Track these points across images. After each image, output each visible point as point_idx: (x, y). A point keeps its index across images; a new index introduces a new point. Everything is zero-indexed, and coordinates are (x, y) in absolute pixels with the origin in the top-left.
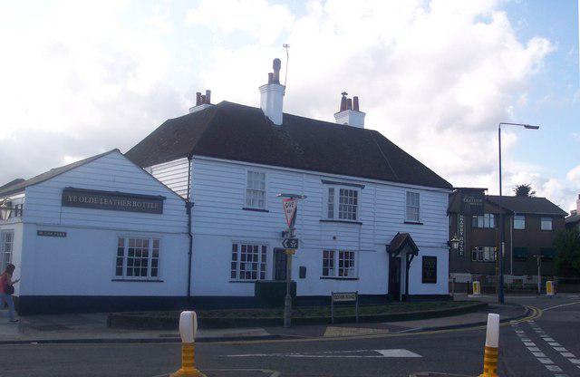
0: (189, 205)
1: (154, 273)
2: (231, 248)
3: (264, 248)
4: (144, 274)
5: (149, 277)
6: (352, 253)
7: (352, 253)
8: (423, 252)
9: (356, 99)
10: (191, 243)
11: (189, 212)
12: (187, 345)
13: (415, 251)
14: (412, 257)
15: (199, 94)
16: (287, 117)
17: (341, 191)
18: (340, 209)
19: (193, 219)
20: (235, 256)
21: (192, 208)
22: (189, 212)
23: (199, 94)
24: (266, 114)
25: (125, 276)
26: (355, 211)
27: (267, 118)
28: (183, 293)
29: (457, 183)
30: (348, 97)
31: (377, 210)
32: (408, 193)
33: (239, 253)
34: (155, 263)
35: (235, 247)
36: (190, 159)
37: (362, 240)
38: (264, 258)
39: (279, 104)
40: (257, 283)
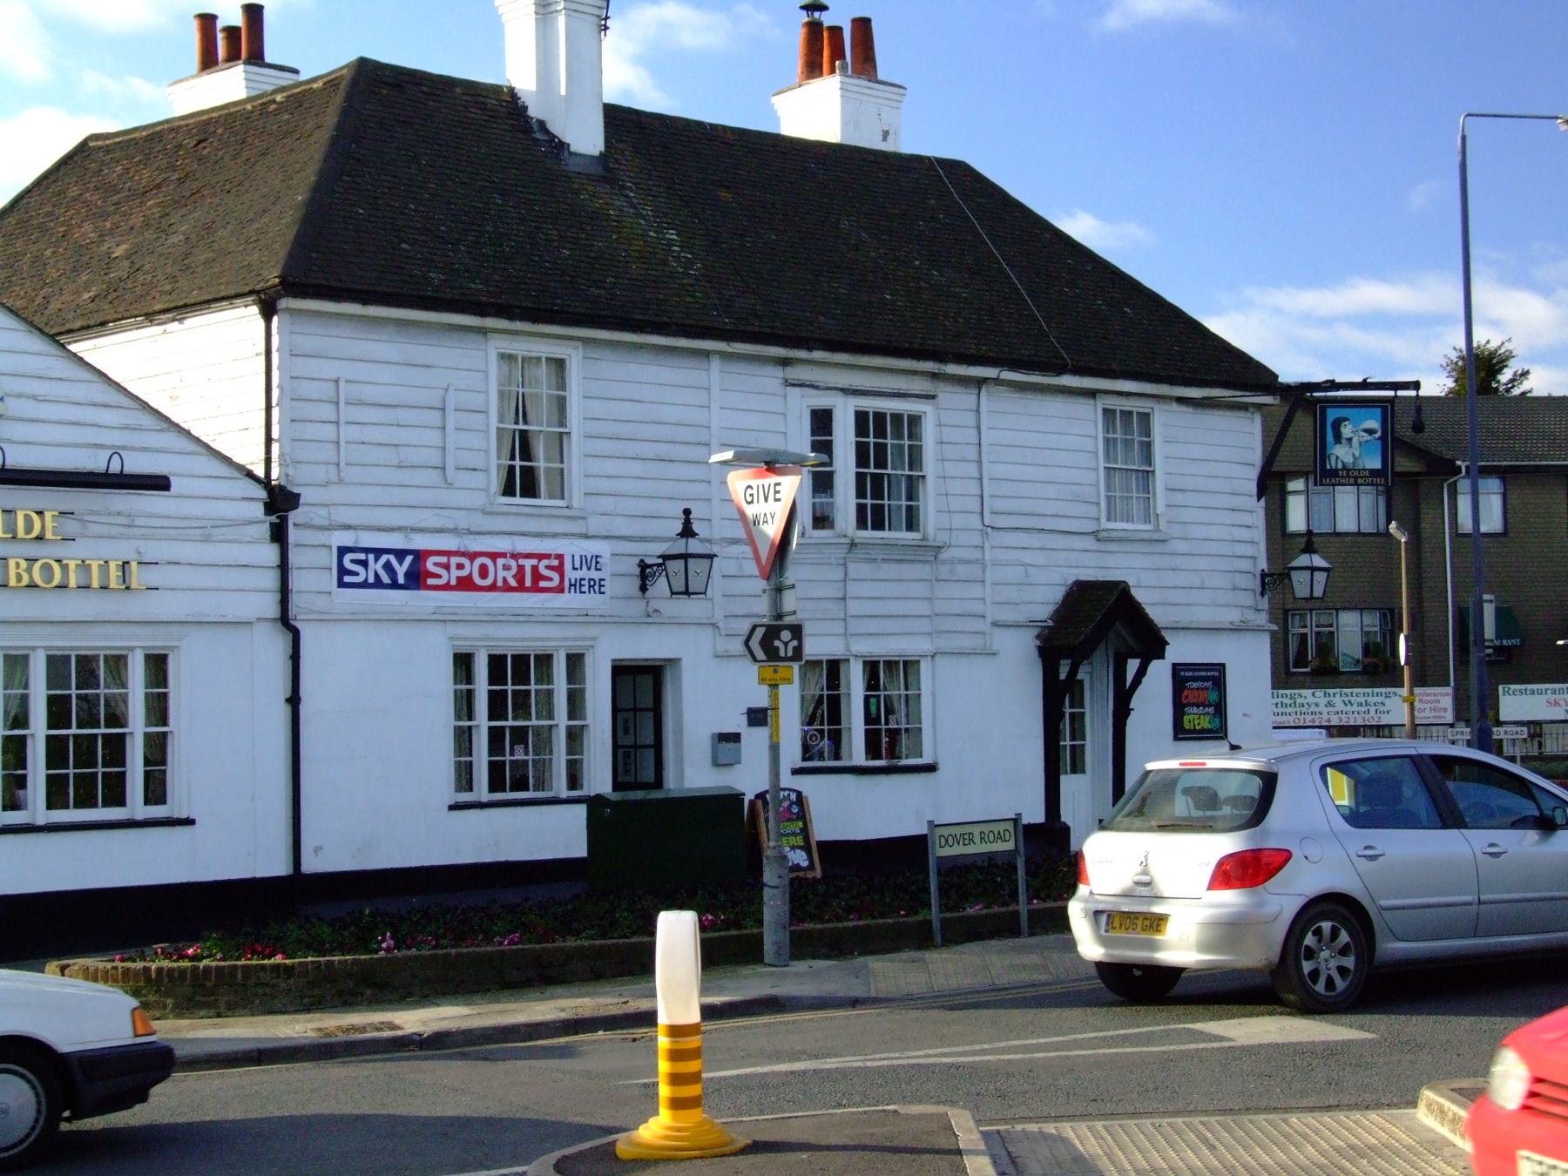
0: (280, 501)
1: (156, 791)
2: (447, 667)
3: (575, 662)
4: (116, 797)
5: (136, 807)
6: (910, 666)
7: (910, 666)
8: (1180, 650)
9: (863, 26)
10: (295, 657)
11: (279, 535)
12: (1251, 838)
13: (1151, 643)
14: (1141, 672)
15: (207, 22)
16: (618, 119)
17: (861, 418)
18: (861, 493)
19: (295, 557)
20: (465, 704)
21: (294, 517)
22: (279, 535)
23: (207, 22)
24: (534, 112)
25: (37, 808)
26: (911, 495)
27: (542, 124)
28: (275, 865)
29: (1290, 371)
30: (828, 19)
31: (347, 433)
32: (1108, 413)
33: (482, 686)
34: (157, 750)
35: (463, 663)
36: (268, 312)
37: (854, 607)
38: (576, 702)
39: (586, 66)
40: (595, 804)
